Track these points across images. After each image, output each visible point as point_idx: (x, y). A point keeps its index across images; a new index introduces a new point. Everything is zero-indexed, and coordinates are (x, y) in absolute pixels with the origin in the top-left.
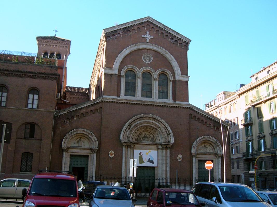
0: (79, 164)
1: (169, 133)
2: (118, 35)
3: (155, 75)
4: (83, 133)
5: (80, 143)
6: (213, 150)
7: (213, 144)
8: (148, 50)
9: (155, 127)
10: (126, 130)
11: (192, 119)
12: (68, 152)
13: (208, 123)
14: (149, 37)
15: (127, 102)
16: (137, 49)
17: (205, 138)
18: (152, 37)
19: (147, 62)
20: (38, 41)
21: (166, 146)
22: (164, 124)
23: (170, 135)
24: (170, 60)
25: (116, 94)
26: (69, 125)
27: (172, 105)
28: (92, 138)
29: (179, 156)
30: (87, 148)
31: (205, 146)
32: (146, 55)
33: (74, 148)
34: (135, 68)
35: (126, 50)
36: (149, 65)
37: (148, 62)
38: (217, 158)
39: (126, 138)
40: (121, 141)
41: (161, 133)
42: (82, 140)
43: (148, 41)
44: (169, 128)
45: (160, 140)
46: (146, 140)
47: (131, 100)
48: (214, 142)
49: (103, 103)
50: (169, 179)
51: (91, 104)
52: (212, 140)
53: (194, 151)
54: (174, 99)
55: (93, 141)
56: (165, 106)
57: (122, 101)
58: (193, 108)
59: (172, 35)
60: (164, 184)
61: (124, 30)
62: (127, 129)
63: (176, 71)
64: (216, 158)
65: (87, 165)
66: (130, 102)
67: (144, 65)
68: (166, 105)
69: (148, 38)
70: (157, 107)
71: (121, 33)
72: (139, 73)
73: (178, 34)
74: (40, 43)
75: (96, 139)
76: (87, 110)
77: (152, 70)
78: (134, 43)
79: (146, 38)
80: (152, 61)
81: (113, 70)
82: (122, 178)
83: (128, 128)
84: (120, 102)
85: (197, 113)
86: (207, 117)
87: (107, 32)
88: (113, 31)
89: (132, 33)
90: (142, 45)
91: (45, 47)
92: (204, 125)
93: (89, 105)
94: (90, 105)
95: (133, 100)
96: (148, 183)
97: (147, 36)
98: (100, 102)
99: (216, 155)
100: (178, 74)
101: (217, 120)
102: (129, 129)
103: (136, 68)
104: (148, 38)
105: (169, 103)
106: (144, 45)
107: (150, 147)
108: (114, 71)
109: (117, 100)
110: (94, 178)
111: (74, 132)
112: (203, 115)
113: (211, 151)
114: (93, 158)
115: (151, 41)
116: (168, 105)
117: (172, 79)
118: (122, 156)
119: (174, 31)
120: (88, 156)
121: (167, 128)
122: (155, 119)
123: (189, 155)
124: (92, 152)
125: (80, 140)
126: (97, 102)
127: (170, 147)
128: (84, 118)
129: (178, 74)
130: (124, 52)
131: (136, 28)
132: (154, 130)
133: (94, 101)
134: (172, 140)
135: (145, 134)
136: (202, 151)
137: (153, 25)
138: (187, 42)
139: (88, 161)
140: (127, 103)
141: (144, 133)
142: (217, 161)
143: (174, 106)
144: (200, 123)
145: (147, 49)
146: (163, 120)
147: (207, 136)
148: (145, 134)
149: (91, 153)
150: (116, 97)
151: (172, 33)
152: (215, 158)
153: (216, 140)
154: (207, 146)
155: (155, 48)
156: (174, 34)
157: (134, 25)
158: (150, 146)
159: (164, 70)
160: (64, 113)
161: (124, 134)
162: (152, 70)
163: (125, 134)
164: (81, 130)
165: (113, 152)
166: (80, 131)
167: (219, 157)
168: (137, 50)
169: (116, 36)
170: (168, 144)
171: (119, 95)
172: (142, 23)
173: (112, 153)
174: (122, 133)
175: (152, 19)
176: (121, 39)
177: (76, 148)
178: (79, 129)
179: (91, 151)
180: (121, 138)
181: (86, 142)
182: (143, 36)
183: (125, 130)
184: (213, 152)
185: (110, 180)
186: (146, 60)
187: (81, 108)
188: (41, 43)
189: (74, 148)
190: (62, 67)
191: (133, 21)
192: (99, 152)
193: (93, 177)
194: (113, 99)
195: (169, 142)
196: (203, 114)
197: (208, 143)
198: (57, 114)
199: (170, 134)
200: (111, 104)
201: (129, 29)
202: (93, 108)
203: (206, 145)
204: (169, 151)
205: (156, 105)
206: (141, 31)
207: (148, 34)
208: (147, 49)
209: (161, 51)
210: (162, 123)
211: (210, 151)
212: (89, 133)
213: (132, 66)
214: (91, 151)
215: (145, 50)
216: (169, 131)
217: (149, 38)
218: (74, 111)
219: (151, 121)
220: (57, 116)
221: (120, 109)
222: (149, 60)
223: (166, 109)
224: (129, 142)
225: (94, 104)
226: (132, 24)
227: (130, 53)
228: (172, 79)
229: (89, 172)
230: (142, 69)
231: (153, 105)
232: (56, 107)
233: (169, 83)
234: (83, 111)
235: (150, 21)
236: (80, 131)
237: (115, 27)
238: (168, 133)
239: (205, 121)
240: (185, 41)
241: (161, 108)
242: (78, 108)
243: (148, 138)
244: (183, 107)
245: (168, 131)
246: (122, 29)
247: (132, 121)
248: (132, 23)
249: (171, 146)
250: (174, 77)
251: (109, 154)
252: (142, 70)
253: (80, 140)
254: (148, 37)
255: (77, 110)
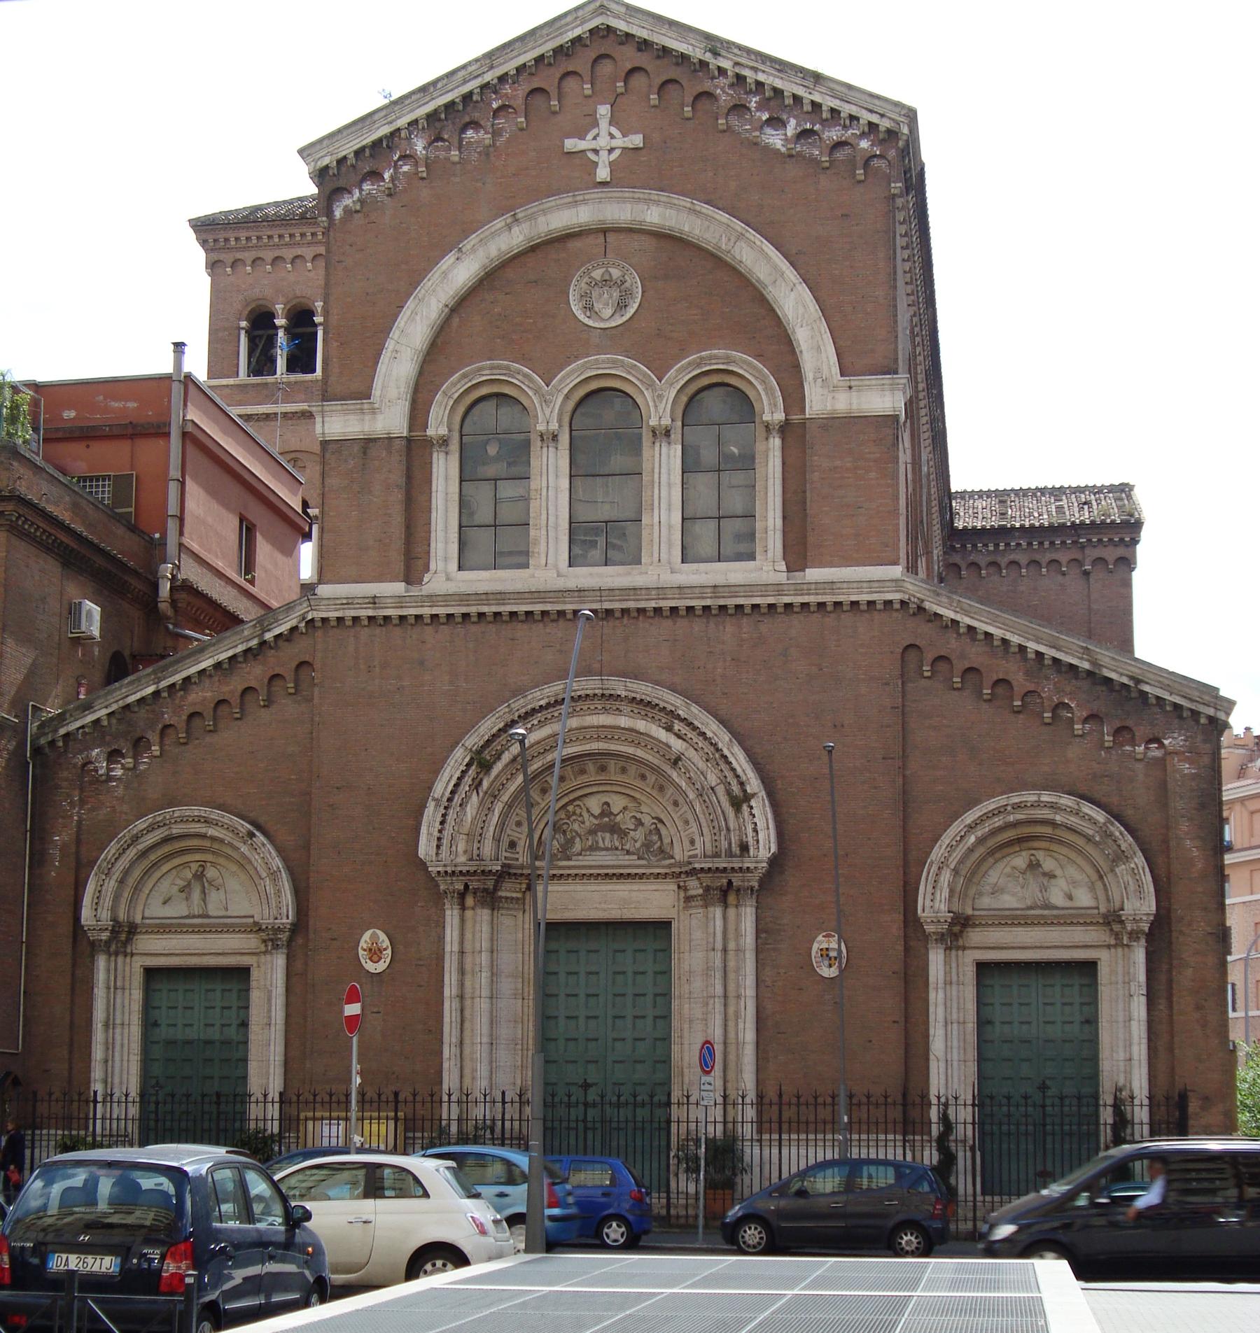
0: (194, 1016)
1: (745, 791)
2: (406, 168)
3: (659, 404)
4: (203, 831)
5: (196, 894)
6: (1092, 888)
7: (1090, 849)
8: (611, 237)
9: (650, 758)
10: (453, 792)
11: (923, 682)
12: (958, 948)
13: (1048, 690)
14: (614, 143)
15: (464, 610)
16: (532, 239)
17: (1017, 807)
18: (637, 140)
19: (602, 325)
20: (203, 243)
21: (725, 881)
22: (709, 734)
23: (753, 803)
24: (759, 281)
25: (399, 567)
26: (126, 788)
27: (771, 600)
28: (256, 859)
29: (825, 946)
30: (238, 921)
31: (1034, 866)
32: (597, 274)
33: (165, 928)
34: (522, 379)
35: (453, 266)
36: (614, 338)
37: (607, 317)
38: (1119, 944)
39: (461, 847)
40: (423, 865)
41: (692, 796)
42: (211, 873)
43: (603, 174)
44: (739, 759)
45: (692, 842)
46: (607, 849)
47: (486, 597)
48: (1091, 832)
49: (319, 633)
50: (751, 1096)
51: (240, 648)
52: (1073, 820)
53: (934, 904)
54: (797, 553)
55: (264, 875)
56: (723, 608)
57: (435, 611)
58: (927, 605)
59: (778, 92)
60: (719, 1134)
61: (438, 125)
62: (465, 787)
63: (805, 353)
64: (1115, 946)
65: (1088, 1022)
66: (485, 609)
67: (579, 342)
68: (731, 602)
69: (604, 154)
70: (669, 623)
71: (419, 146)
72: (549, 409)
73: (817, 78)
74: (215, 256)
75: (277, 862)
76: (225, 689)
77: (626, 370)
78: (508, 206)
79: (591, 156)
80: (636, 306)
81: (374, 411)
82: (445, 1098)
83: (468, 780)
84: (418, 618)
85: (959, 634)
86: (1039, 654)
87: (326, 161)
88: (363, 149)
89: (496, 133)
90: (558, 208)
91: (311, 275)
92: (1019, 712)
93: (230, 653)
94: (234, 657)
95: (501, 596)
96: (556, 1124)
97: (595, 138)
98: (294, 629)
99: (1116, 927)
100: (818, 370)
101: (1113, 676)
102: (477, 785)
103: (525, 375)
104: (604, 154)
105: (764, 588)
106: (575, 203)
107: (634, 894)
108: (380, 417)
109: (400, 601)
110: (57, 1101)
111: (151, 829)
112: (1005, 641)
113: (1084, 899)
114: (271, 976)
115: (632, 173)
116: (741, 601)
117: (773, 413)
118: (440, 958)
119: (782, 67)
120: (1089, 967)
121: (731, 759)
122: (644, 706)
123: (896, 929)
124: (1117, 936)
125: (199, 876)
126: (277, 631)
127: (752, 888)
128: (208, 739)
129: (818, 370)
130: (442, 282)
131: (516, 93)
132: (651, 778)
133: (255, 626)
134: (761, 836)
135: (606, 811)
136: (1009, 901)
137: (640, 50)
138: (885, 124)
139: (248, 999)
140: (466, 616)
141: (594, 804)
142: (1120, 970)
143: (788, 606)
144: (985, 701)
145: (605, 231)
146: (695, 709)
147: (1030, 797)
148: (606, 811)
149: (1113, 942)
150: (399, 588)
151: (771, 79)
152: (1109, 947)
153: (1100, 816)
154: (1048, 864)
155: (654, 216)
156: (790, 87)
157: (502, 79)
158: (636, 886)
159: (718, 356)
160: (90, 718)
161: (442, 823)
162: (626, 370)
163: (449, 818)
164: (186, 817)
165: (382, 936)
166: (183, 820)
167: (1134, 936)
168: (533, 249)
169: (387, 176)
170: (736, 866)
171: (413, 565)
172: (558, 51)
173: (374, 949)
174: (431, 814)
175: (623, 10)
176: (425, 193)
177: (180, 925)
178: (178, 811)
179: (1111, 930)
180: (425, 848)
181: (233, 884)
182: (571, 144)
183: (447, 794)
184: (1097, 908)
185: (318, 1114)
186: (597, 306)
187: (187, 679)
188: (222, 256)
189: (161, 926)
190: (165, 424)
191: (490, 55)
192: (295, 938)
193: (54, 1097)
194: (374, 601)
195: (744, 848)
196: (1008, 636)
197: (1051, 839)
198: (47, 730)
199: (747, 797)
200: (365, 633)
201: (476, 115)
202: (254, 674)
203: (1040, 855)
204: (747, 917)
205: (658, 611)
206: (555, 113)
207: (604, 124)
208: (604, 231)
209: (697, 232)
210: (690, 724)
211: (1070, 898)
212: (234, 831)
213: (499, 367)
214: (1111, 930)
215: (590, 240)
216: (744, 778)
217: (611, 150)
218: (142, 700)
219: (624, 722)
220: (52, 743)
221: (422, 663)
222: (621, 306)
223: (729, 630)
224: (472, 869)
225: (263, 643)
226: (488, 77)
227: (489, 280)
228: (773, 413)
229: (253, 1067)
230: (561, 381)
231: (641, 611)
232: (80, 685)
233: (760, 447)
234: (202, 696)
235: (614, 23)
236: (183, 820)
237: (376, 117)
238: (736, 789)
239: (1020, 681)
240: (875, 119)
241: (698, 626)
242: (164, 684)
243: (623, 834)
244: (855, 604)
245: (738, 777)
246: (423, 123)
247: (495, 730)
248: (492, 68)
249: (762, 882)
250: (794, 395)
251: (361, 952)
252: (570, 378)
253: (199, 876)
254: (605, 141)
255: (165, 694)
